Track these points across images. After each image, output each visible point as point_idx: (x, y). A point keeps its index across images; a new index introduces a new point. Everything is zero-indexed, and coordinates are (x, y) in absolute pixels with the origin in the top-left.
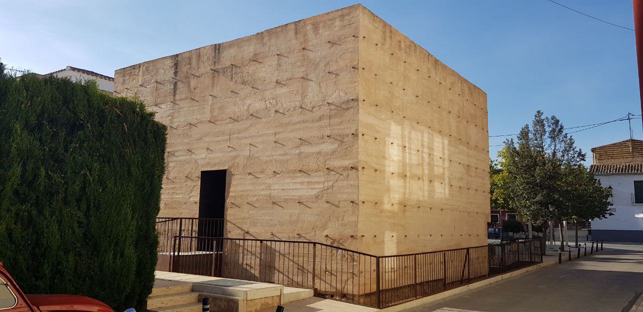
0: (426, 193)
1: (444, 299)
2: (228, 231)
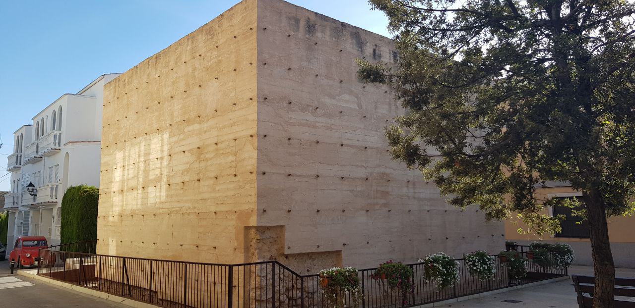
0: (139, 201)
1: (56, 285)
2: (255, 103)
